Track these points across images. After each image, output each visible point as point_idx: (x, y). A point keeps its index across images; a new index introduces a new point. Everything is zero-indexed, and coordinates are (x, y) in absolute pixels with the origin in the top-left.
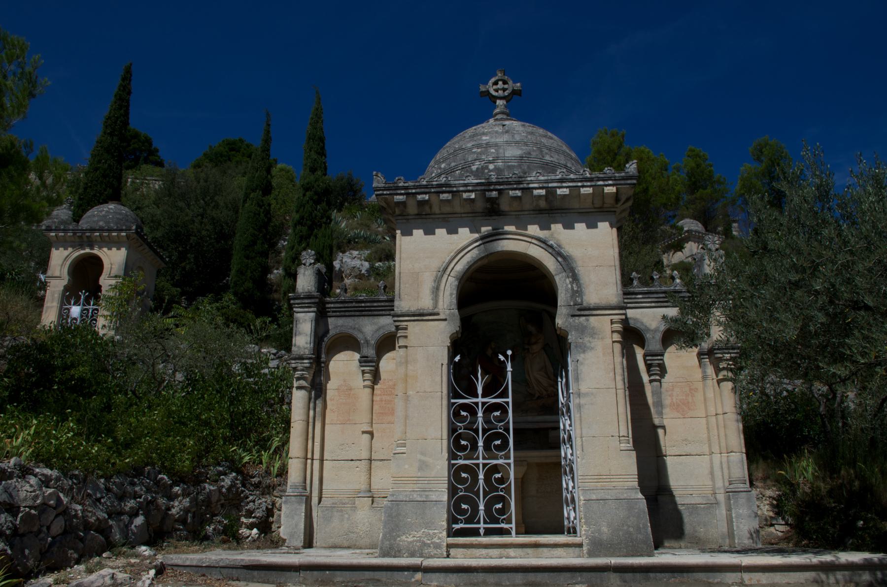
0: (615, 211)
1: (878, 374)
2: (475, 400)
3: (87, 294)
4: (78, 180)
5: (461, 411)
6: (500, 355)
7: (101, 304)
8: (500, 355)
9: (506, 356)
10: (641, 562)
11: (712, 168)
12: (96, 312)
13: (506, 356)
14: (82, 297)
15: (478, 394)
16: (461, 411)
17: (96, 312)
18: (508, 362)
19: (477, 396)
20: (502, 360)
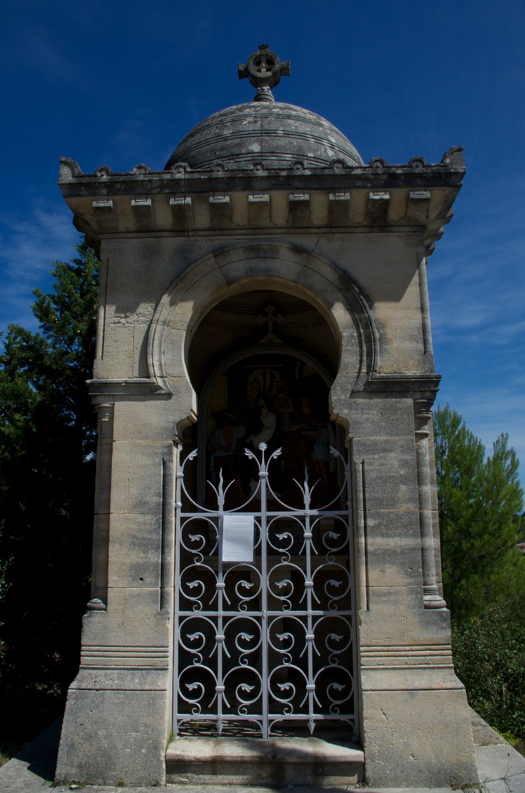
0: (425, 608)
1: (70, 325)
2: (300, 512)
3: (277, 453)
4: (416, 351)
5: (188, 584)
6: (246, 450)
7: (439, 433)
8: (246, 450)
9: (258, 452)
10: (166, 716)
11: (267, 50)
12: (335, 583)
13: (258, 452)
14: (263, 471)
15: (304, 505)
16: (188, 584)
17: (335, 583)
18: (261, 464)
19: (303, 507)
20: (250, 458)
